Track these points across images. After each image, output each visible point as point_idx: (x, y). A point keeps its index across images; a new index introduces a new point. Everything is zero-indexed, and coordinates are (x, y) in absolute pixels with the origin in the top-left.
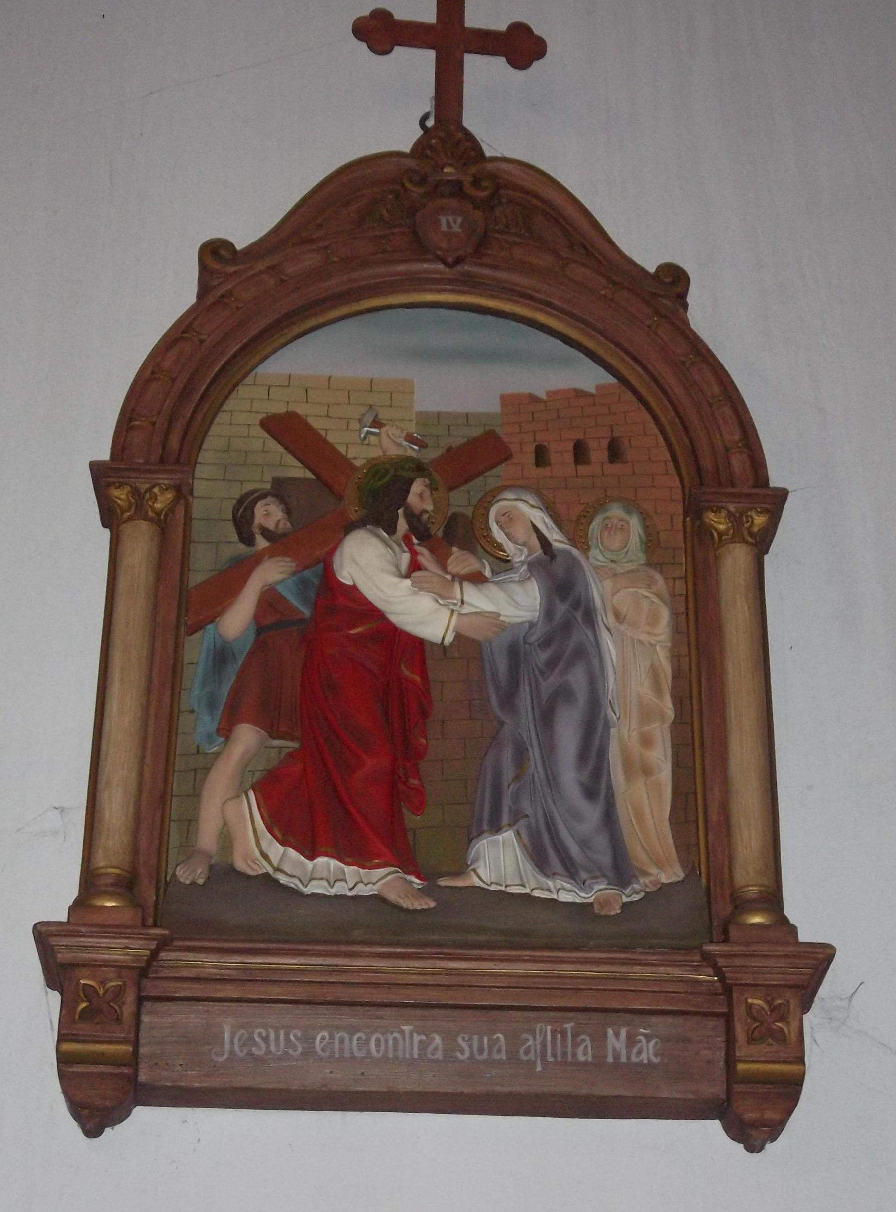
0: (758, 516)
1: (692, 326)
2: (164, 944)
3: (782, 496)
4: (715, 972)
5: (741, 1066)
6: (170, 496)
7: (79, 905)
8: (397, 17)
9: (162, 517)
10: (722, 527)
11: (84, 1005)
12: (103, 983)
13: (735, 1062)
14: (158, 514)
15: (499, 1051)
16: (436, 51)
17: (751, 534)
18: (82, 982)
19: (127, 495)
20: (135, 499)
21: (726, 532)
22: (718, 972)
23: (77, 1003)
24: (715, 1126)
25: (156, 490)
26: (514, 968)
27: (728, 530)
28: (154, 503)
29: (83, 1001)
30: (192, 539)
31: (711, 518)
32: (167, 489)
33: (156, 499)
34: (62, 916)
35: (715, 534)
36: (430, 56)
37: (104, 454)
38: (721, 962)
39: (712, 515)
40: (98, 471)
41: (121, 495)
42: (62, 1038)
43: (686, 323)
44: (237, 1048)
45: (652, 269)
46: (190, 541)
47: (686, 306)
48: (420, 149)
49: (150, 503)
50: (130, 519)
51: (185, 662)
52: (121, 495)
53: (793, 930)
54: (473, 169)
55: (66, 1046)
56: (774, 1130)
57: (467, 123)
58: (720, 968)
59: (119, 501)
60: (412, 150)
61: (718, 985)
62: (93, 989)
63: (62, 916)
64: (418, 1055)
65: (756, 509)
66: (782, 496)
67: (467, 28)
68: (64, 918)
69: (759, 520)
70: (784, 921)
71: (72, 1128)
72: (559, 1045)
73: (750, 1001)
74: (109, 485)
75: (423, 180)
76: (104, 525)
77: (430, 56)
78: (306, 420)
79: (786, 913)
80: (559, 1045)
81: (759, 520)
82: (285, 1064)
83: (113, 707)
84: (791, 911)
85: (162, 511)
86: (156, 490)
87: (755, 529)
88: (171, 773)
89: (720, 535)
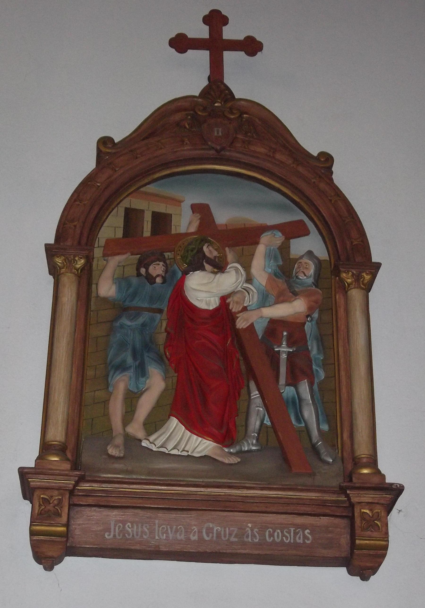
0: (367, 275)
2: (81, 479)
3: (378, 266)
4: (345, 496)
5: (358, 542)
6: (83, 261)
7: (40, 458)
8: (189, 36)
10: (349, 281)
13: (355, 540)
15: (247, 537)
16: (149, 237)
17: (363, 284)
18: (42, 496)
21: (351, 283)
24: (344, 570)
25: (77, 259)
26: (249, 493)
27: (352, 282)
28: (75, 265)
33: (77, 263)
34: (32, 465)
36: (206, 53)
37: (51, 240)
39: (344, 275)
40: (48, 248)
41: (59, 261)
43: (332, 180)
44: (117, 534)
45: (315, 154)
47: (332, 173)
48: (205, 93)
49: (74, 265)
51: (92, 297)
54: (229, 105)
56: (374, 570)
57: (226, 81)
58: (349, 494)
60: (199, 95)
62: (47, 500)
63: (32, 465)
65: (366, 272)
66: (378, 266)
67: (225, 40)
69: (367, 277)
75: (205, 109)
76: (50, 273)
77: (206, 53)
78: (137, 263)
79: (379, 468)
81: (367, 277)
82: (128, 513)
84: (382, 466)
85: (79, 268)
86: (77, 259)
87: (366, 281)
89: (349, 285)
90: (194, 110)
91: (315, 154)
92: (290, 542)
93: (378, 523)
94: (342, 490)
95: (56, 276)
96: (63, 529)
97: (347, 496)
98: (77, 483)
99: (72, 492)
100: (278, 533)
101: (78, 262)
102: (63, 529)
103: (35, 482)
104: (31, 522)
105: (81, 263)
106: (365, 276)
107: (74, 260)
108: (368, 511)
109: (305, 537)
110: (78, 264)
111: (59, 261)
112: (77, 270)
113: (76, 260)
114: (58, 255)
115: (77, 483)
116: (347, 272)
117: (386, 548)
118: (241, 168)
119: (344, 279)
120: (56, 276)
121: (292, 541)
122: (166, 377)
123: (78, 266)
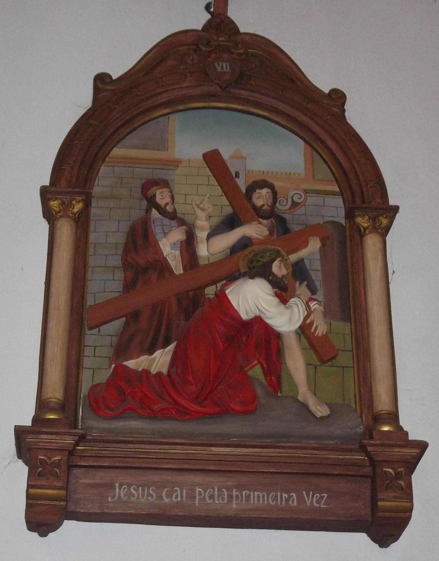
1: (348, 120)
3: (396, 209)
5: (380, 503)
7: (35, 420)
9: (77, 216)
10: (365, 225)
11: (40, 469)
12: (50, 458)
14: (75, 214)
15: (177, 497)
18: (40, 457)
19: (59, 205)
20: (63, 207)
21: (368, 228)
22: (367, 453)
23: (37, 468)
24: (362, 537)
25: (74, 202)
29: (40, 468)
30: (88, 292)
31: (359, 220)
32: (79, 202)
33: (74, 207)
35: (362, 229)
38: (369, 449)
42: (29, 486)
45: (327, 91)
46: (87, 293)
48: (207, 27)
50: (61, 217)
52: (54, 204)
53: (406, 433)
55: (32, 491)
59: (54, 208)
61: (368, 462)
64: (198, 504)
66: (396, 209)
68: (31, 425)
69: (385, 222)
70: (401, 428)
71: (16, 425)
72: (266, 500)
73: (384, 469)
74: (50, 199)
75: (208, 44)
80: (266, 500)
81: (385, 222)
83: (52, 324)
87: (383, 225)
88: (81, 369)
89: (365, 229)
90: (197, 45)
91: (327, 91)
92: (181, 500)
93: (57, 470)
94: (363, 448)
95: (51, 222)
96: (62, 493)
97: (367, 453)
98: (77, 444)
99: (71, 453)
100: (273, 495)
101: (75, 206)
102: (62, 493)
103: (30, 439)
104: (28, 485)
105: (78, 207)
106: (382, 220)
107: (71, 203)
108: (390, 470)
109: (149, 495)
110: (76, 208)
111: (54, 204)
112: (382, 229)
113: (73, 204)
114: (54, 199)
115: (77, 444)
116: (363, 217)
117: (411, 510)
118: (239, 104)
119: (360, 224)
120: (51, 222)
121: (266, 503)
122: (72, 316)
123: (75, 210)
